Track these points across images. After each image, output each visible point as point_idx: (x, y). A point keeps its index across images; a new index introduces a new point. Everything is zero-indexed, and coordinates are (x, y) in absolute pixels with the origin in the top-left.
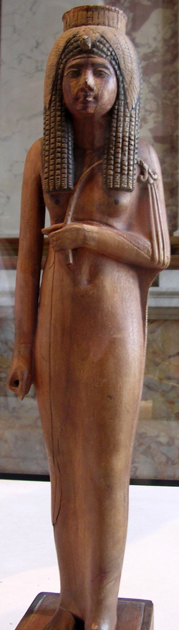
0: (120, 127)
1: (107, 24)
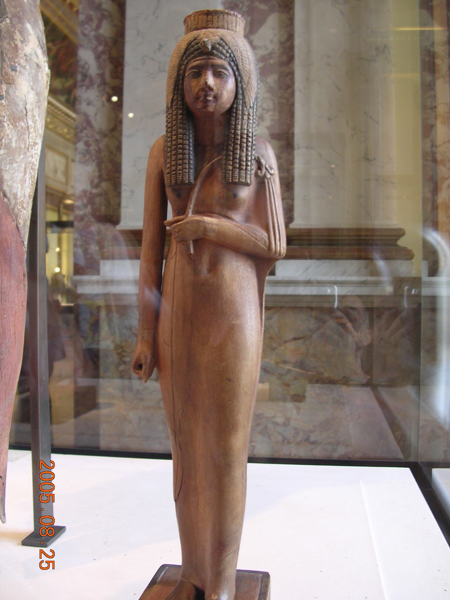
0: (238, 124)
1: (226, 28)
